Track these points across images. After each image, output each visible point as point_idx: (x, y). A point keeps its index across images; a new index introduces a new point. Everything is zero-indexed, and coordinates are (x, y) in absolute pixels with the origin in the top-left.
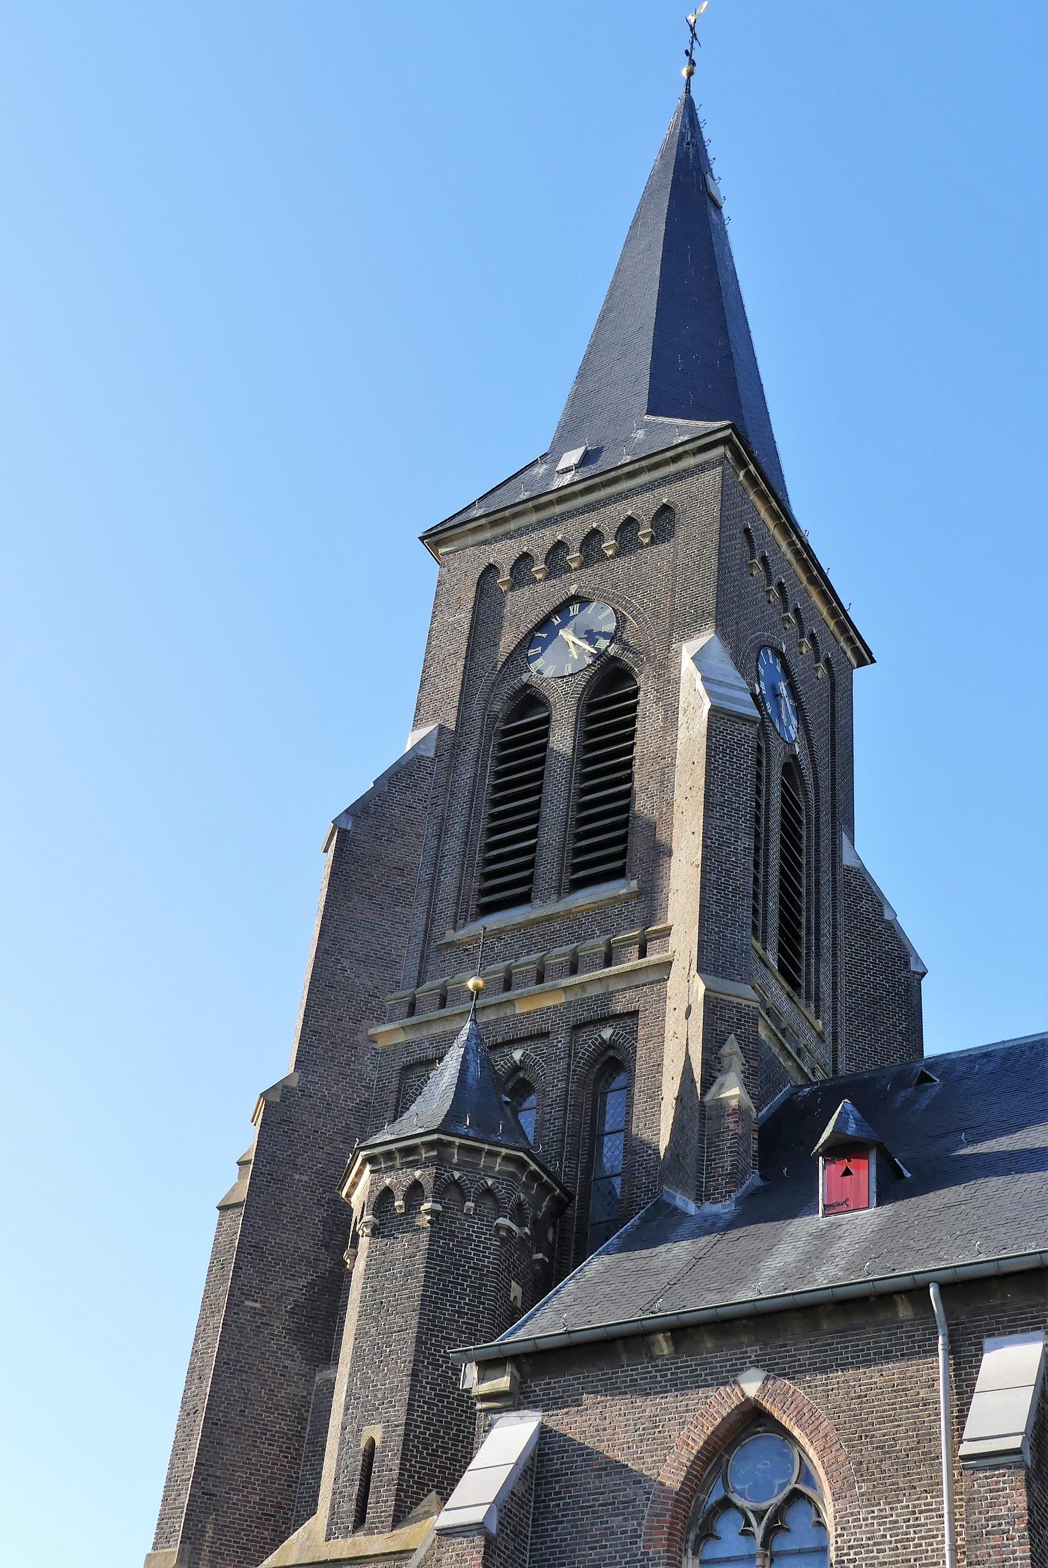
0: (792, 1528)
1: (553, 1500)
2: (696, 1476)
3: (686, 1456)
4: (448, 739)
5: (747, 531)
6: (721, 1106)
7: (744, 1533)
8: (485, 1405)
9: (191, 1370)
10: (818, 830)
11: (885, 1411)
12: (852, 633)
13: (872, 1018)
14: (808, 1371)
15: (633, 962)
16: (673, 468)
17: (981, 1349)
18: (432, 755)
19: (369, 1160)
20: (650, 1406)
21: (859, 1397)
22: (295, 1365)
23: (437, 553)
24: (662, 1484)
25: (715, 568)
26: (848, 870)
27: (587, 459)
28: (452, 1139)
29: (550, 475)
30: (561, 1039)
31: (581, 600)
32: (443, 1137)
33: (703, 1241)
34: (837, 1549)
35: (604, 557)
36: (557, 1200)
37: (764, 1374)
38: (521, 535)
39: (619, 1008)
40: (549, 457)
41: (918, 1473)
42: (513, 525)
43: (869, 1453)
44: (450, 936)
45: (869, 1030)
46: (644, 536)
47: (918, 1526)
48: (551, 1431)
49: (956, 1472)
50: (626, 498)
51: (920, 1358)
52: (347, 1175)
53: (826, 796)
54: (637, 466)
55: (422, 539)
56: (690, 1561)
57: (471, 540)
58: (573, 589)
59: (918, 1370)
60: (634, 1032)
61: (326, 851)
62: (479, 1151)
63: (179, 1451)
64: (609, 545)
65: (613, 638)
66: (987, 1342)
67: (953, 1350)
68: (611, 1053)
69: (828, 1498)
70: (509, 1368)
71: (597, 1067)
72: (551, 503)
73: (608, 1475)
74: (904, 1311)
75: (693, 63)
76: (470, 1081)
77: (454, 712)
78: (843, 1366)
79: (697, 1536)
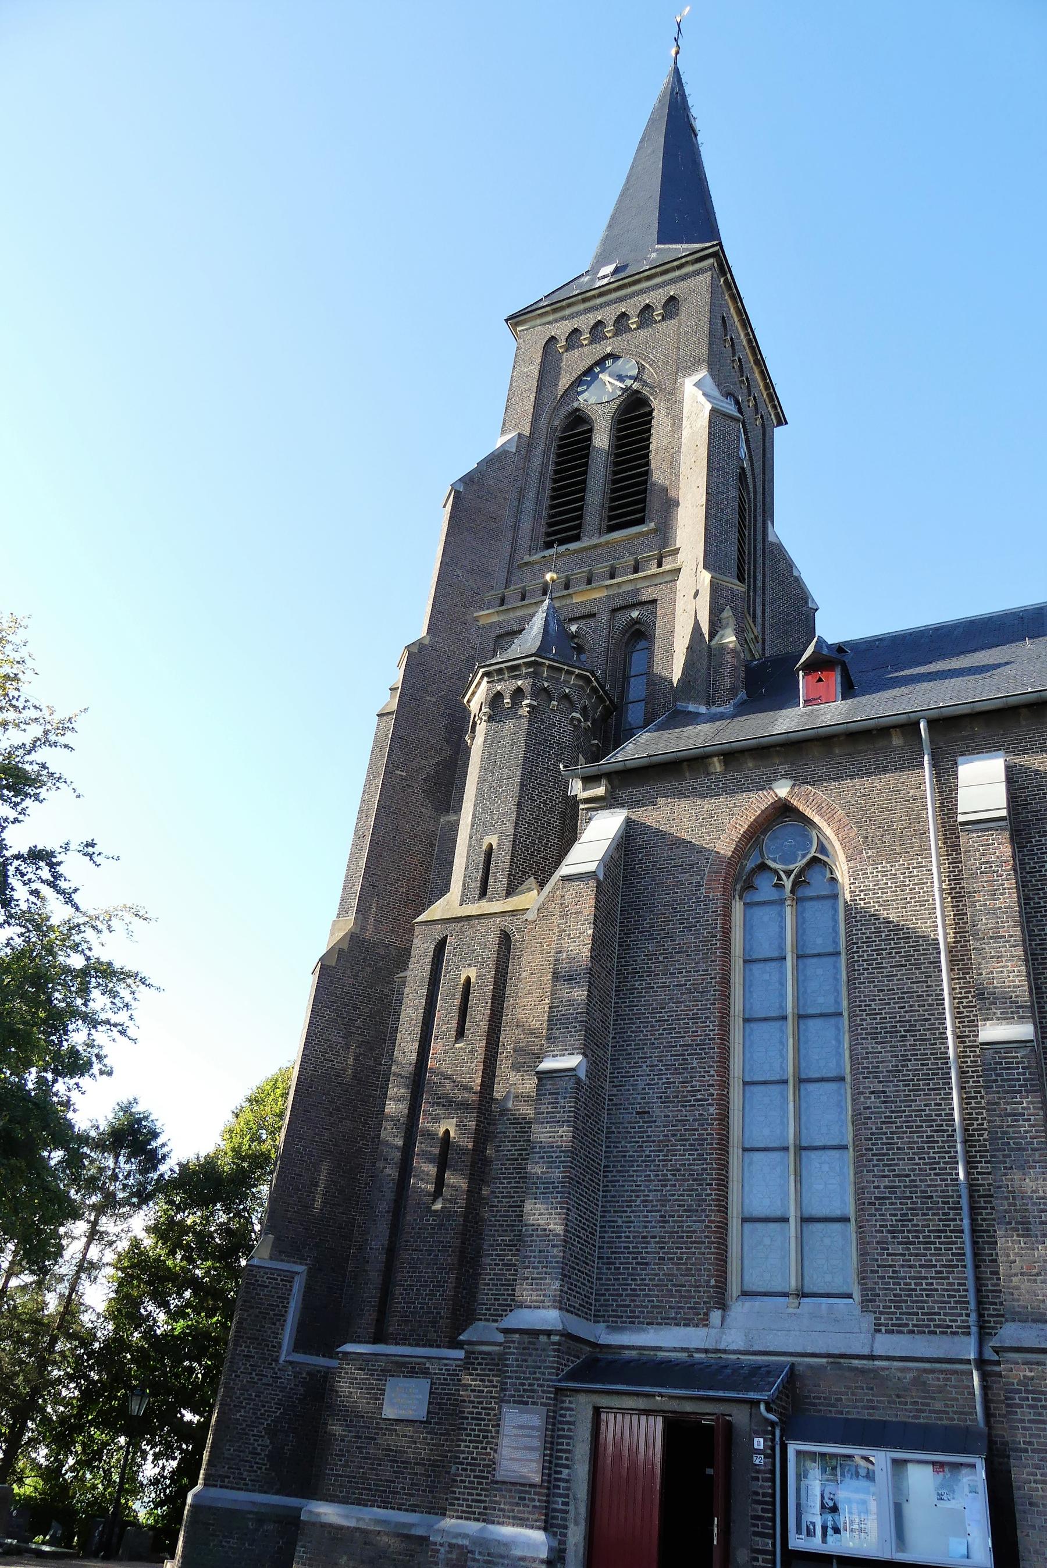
0: (812, 882)
1: (638, 864)
2: (741, 848)
3: (736, 835)
4: (525, 441)
5: (723, 318)
6: (722, 648)
7: (776, 886)
8: (586, 806)
9: (361, 812)
10: (755, 517)
11: (884, 804)
12: (776, 402)
13: (785, 632)
14: (826, 780)
15: (654, 569)
16: (677, 273)
17: (956, 764)
18: (514, 450)
19: (486, 674)
20: (707, 805)
21: (865, 795)
22: (428, 811)
23: (515, 330)
24: (719, 853)
25: (707, 332)
26: (772, 544)
27: (616, 271)
28: (544, 661)
29: (592, 281)
30: (604, 618)
31: (614, 356)
32: (538, 659)
33: (718, 723)
34: (851, 892)
35: (630, 330)
36: (605, 708)
37: (791, 783)
38: (573, 318)
39: (644, 598)
40: (593, 271)
41: (911, 843)
42: (567, 312)
43: (873, 831)
44: (527, 558)
45: (783, 640)
46: (657, 315)
47: (912, 876)
48: (634, 821)
49: (940, 842)
50: (645, 292)
51: (909, 770)
52: (469, 687)
53: (760, 497)
54: (653, 271)
55: (506, 320)
56: (738, 903)
57: (538, 321)
58: (608, 350)
59: (908, 778)
60: (654, 614)
61: (444, 507)
62: (561, 670)
63: (353, 860)
64: (633, 322)
65: (635, 379)
66: (960, 759)
67: (935, 765)
68: (637, 626)
69: (841, 857)
70: (604, 782)
71: (628, 635)
72: (594, 297)
73: (677, 848)
74: (897, 741)
75: (678, 46)
76: (551, 631)
77: (529, 425)
78: (852, 777)
79: (742, 887)
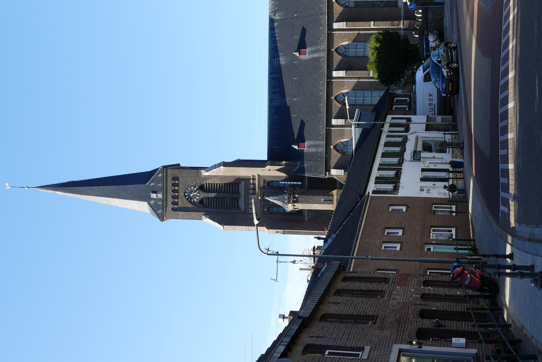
42: (165, 206)
57: (165, 213)
58: (182, 194)
67: (332, 127)
